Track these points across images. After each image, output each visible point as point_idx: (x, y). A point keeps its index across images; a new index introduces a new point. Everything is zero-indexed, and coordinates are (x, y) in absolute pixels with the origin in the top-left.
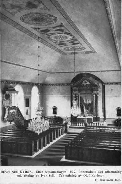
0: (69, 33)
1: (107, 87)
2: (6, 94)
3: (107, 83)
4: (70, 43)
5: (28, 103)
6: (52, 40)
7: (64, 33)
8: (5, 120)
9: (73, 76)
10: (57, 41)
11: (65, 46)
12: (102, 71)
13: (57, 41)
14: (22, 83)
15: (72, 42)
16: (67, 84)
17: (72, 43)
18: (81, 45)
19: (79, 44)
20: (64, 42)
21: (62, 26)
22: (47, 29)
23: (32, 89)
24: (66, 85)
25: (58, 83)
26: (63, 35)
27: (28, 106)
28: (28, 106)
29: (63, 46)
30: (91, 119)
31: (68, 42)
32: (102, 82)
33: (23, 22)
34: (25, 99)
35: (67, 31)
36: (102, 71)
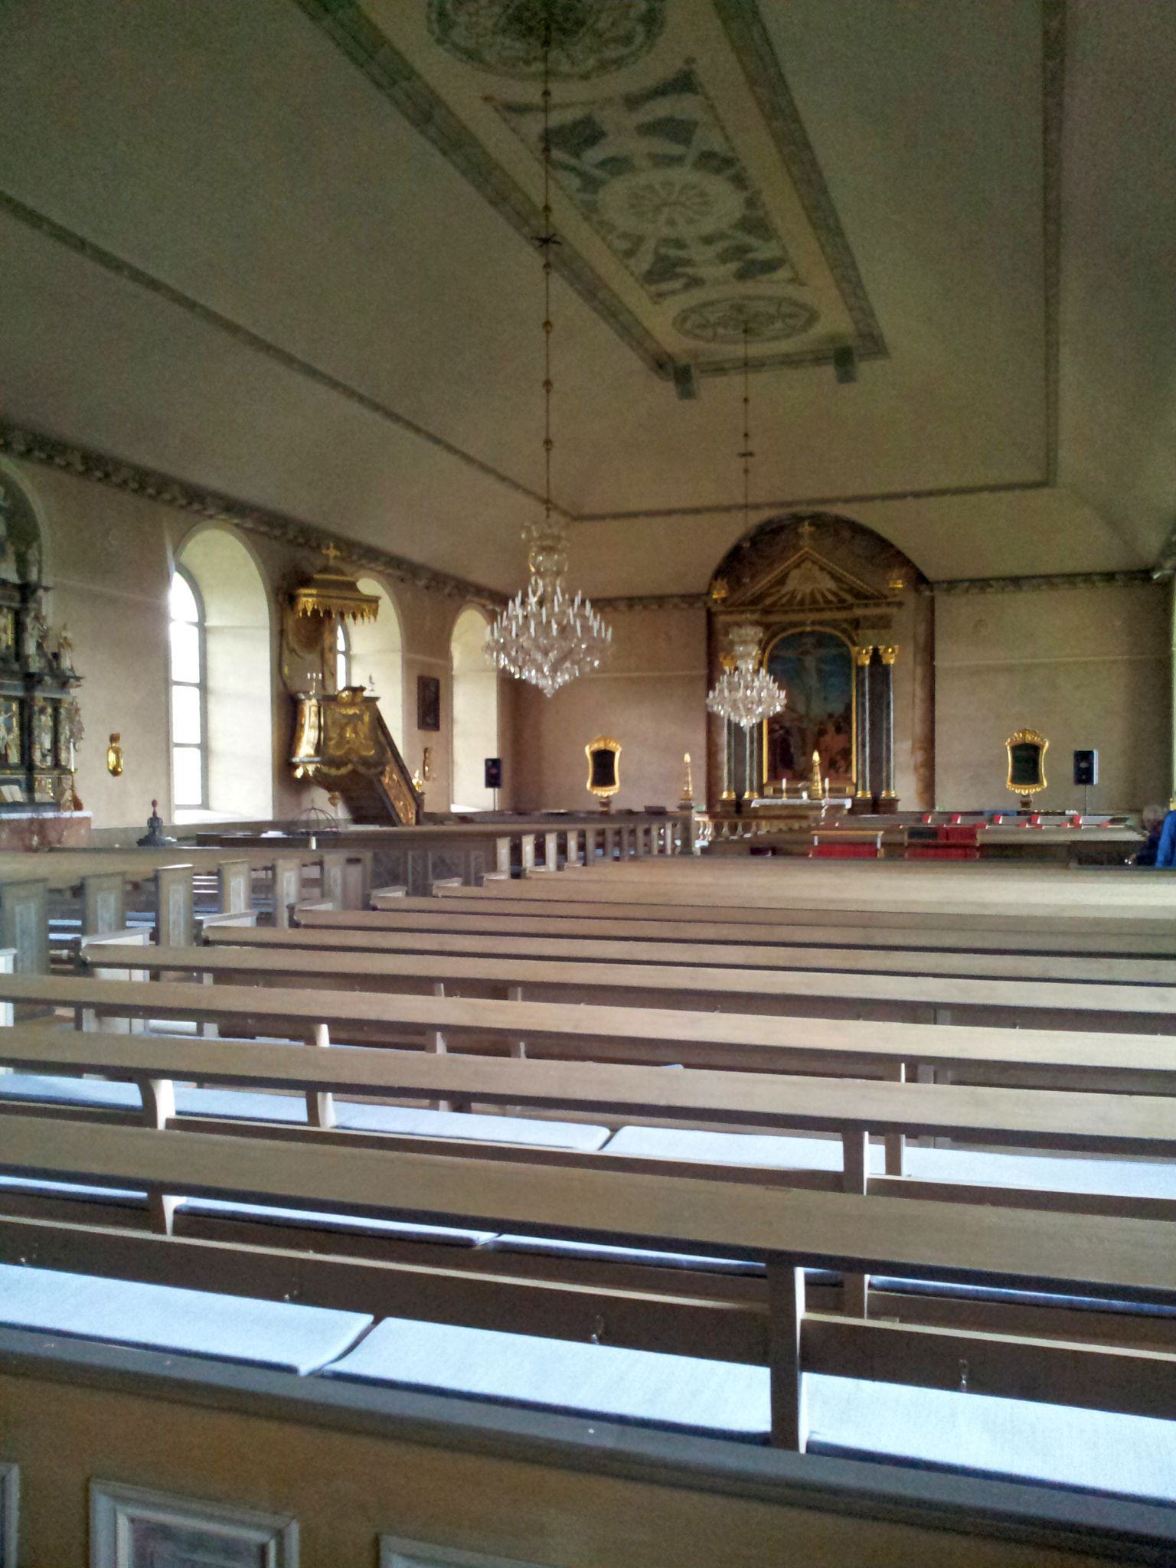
0: (728, 162)
1: (942, 602)
2: (300, 607)
3: (952, 584)
4: (724, 258)
5: (430, 705)
6: (604, 228)
7: (692, 155)
8: (299, 773)
9: (732, 531)
10: (640, 239)
11: (687, 287)
12: (917, 495)
13: (640, 239)
14: (402, 572)
15: (741, 250)
16: (684, 597)
17: (733, 266)
18: (792, 281)
19: (783, 274)
20: (681, 253)
21: (684, 83)
22: (587, 121)
23: (457, 631)
24: (676, 606)
25: (624, 592)
26: (684, 175)
27: (435, 726)
28: (435, 726)
29: (673, 292)
30: (807, 1276)
31: (711, 251)
32: (919, 580)
33: (440, 42)
34: (416, 673)
35: (717, 144)
36: (917, 495)
